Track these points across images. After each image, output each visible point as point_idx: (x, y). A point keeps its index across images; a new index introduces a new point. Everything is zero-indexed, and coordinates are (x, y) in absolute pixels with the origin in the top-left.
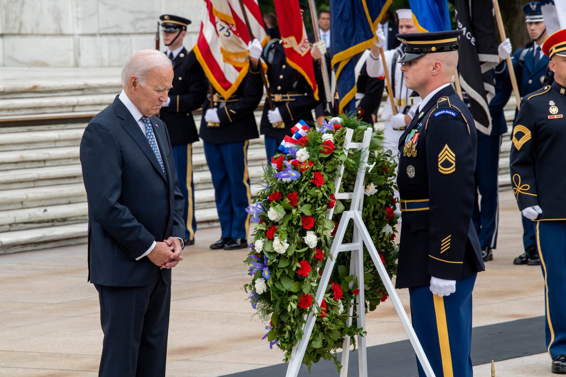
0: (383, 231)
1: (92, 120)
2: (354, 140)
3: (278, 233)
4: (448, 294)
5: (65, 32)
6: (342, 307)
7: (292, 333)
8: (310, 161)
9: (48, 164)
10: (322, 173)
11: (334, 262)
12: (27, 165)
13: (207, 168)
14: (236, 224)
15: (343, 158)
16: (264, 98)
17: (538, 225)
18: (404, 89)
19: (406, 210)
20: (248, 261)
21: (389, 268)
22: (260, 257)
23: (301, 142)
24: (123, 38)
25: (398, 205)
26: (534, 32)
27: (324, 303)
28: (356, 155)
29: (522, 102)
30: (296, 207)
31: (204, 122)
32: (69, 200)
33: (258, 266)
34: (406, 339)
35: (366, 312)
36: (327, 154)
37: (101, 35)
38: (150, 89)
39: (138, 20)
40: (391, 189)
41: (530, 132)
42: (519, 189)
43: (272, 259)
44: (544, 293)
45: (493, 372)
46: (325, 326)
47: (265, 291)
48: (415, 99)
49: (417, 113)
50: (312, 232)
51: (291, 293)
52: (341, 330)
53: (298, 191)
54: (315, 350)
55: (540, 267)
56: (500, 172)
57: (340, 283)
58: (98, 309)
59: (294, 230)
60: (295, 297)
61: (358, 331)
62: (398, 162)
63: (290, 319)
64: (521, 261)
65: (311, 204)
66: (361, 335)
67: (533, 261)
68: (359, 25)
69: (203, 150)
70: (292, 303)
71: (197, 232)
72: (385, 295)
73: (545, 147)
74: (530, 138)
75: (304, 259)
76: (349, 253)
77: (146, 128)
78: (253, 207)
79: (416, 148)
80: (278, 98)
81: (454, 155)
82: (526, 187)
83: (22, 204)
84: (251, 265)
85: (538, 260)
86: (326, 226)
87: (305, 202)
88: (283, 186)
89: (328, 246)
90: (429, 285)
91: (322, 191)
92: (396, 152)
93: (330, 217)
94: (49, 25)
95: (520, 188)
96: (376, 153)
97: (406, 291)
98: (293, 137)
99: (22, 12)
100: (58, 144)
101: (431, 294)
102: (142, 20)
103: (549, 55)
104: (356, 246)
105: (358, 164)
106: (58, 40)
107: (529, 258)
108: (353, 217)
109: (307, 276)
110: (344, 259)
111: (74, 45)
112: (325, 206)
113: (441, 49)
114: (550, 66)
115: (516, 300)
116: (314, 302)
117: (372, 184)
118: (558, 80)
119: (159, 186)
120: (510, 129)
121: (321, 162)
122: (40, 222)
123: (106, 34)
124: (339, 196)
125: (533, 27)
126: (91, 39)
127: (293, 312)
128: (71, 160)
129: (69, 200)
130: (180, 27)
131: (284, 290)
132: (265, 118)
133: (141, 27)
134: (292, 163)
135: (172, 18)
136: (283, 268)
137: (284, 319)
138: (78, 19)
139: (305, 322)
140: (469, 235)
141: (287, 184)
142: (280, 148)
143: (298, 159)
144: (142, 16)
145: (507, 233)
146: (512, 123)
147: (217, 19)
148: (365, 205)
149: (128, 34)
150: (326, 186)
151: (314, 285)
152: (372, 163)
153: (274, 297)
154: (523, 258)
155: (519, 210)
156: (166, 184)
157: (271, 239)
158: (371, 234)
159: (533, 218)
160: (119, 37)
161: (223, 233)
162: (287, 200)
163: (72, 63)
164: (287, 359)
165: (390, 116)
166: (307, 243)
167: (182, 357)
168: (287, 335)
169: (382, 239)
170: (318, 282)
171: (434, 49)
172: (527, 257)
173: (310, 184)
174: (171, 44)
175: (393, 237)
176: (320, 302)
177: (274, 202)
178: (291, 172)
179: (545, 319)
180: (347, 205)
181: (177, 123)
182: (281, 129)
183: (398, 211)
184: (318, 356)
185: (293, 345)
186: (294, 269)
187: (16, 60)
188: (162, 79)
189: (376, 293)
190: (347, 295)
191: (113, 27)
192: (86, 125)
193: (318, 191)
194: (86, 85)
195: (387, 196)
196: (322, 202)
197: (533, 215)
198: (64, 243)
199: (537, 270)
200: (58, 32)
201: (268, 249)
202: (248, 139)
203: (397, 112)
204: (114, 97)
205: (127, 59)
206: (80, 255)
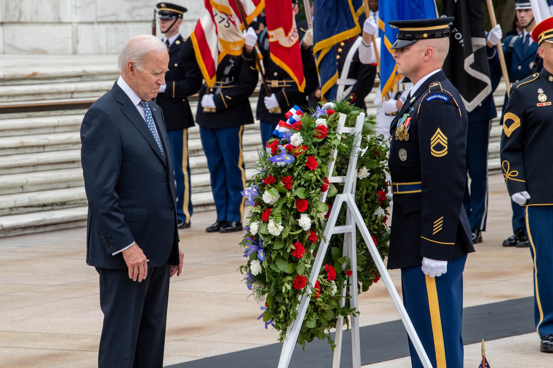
0: (376, 213)
2: (347, 124)
3: (273, 216)
4: (440, 275)
5: (63, 20)
6: (335, 287)
7: (286, 313)
8: (304, 146)
9: (47, 149)
10: (316, 157)
11: (328, 243)
12: (27, 150)
13: (203, 153)
14: (231, 207)
15: (336, 142)
16: (259, 84)
17: (527, 208)
19: (398, 193)
20: (243, 243)
21: (381, 250)
22: (255, 239)
23: (295, 126)
24: (120, 26)
25: (389, 188)
26: (524, 19)
27: (318, 284)
28: (349, 139)
29: (512, 89)
30: (290, 190)
31: (200, 108)
33: (254, 248)
35: (359, 293)
36: (321, 139)
37: (99, 23)
39: (134, 8)
40: (383, 172)
41: (519, 120)
42: (508, 175)
43: (267, 241)
46: (319, 306)
47: (261, 272)
48: (406, 84)
49: (409, 97)
50: (306, 215)
51: (285, 275)
52: (335, 310)
53: (292, 174)
54: (309, 330)
55: (529, 249)
56: (490, 156)
57: (333, 264)
58: (98, 290)
59: (288, 213)
60: (289, 278)
61: (351, 311)
62: (389, 146)
63: (284, 299)
64: (509, 243)
65: (305, 187)
66: (354, 315)
67: (522, 243)
68: (342, 15)
69: (199, 136)
70: (286, 284)
71: (193, 215)
72: (377, 276)
73: (534, 134)
74: (519, 125)
75: (298, 241)
76: (342, 235)
77: (145, 112)
78: (249, 191)
79: (409, 132)
80: (275, 84)
81: (446, 139)
82: (515, 173)
83: (22, 189)
84: (247, 247)
85: (528, 242)
86: (320, 209)
88: (277, 170)
89: (322, 228)
90: (421, 265)
91: (315, 175)
92: (387, 136)
93: (324, 200)
94: (48, 13)
95: (509, 175)
96: (369, 137)
98: (288, 122)
100: (57, 130)
102: (139, 8)
103: (538, 42)
104: (349, 229)
105: (350, 149)
107: (518, 239)
108: (346, 200)
109: (301, 257)
110: (337, 241)
111: (73, 33)
113: (432, 35)
114: (539, 52)
116: (308, 283)
117: (365, 168)
118: (546, 67)
119: (160, 169)
120: (499, 114)
121: (315, 146)
122: (39, 206)
123: (104, 22)
124: (332, 179)
125: (523, 14)
126: (89, 27)
127: (288, 293)
129: (68, 185)
130: (176, 15)
131: (279, 271)
132: (261, 104)
133: (137, 15)
134: (287, 148)
135: (168, 5)
136: (278, 250)
137: (279, 300)
138: (76, 7)
139: (299, 303)
140: (461, 218)
141: (281, 168)
142: (274, 133)
143: (292, 143)
145: (496, 216)
146: (501, 108)
148: (357, 189)
149: (125, 22)
150: (319, 170)
151: (308, 266)
152: (365, 147)
153: (268, 278)
154: (512, 240)
155: (508, 194)
156: (166, 168)
157: (266, 222)
158: (364, 217)
159: (522, 203)
160: (116, 26)
161: (218, 217)
162: (281, 184)
163: (70, 50)
164: (282, 339)
166: (301, 226)
168: (282, 315)
169: (374, 222)
170: (312, 263)
172: (516, 239)
173: (304, 168)
174: (168, 32)
175: (385, 219)
176: (314, 283)
177: (269, 185)
178: (285, 156)
179: (534, 299)
180: (340, 188)
181: (173, 109)
183: (390, 194)
184: (312, 336)
186: (289, 251)
187: (16, 48)
188: (158, 62)
189: (369, 274)
190: (340, 276)
191: (110, 16)
192: (85, 111)
193: (312, 175)
194: (84, 72)
197: (521, 200)
198: (63, 226)
200: (57, 21)
201: (263, 231)
202: (244, 124)
203: (389, 98)
204: (112, 83)
205: (122, 47)
206: (79, 239)
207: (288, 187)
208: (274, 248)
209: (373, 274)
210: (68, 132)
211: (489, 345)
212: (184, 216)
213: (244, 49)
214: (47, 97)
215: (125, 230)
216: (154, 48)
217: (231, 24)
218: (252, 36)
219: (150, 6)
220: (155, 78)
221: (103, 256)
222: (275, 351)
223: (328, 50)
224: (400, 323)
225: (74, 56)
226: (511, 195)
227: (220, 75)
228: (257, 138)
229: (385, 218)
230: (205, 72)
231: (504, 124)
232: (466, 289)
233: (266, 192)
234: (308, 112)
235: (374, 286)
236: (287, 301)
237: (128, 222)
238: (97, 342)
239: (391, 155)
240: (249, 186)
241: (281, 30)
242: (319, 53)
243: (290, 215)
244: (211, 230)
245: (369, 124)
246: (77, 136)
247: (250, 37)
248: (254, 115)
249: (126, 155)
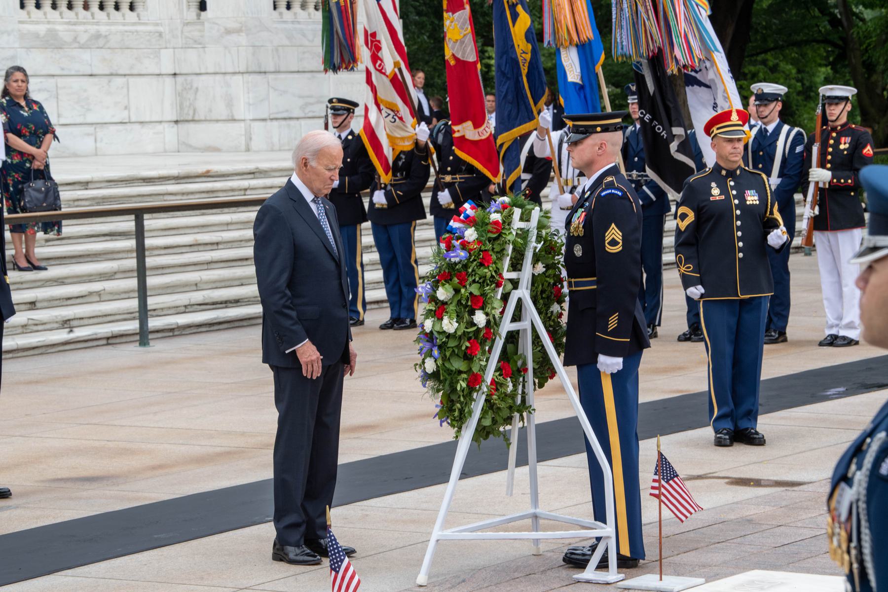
0: (551, 309)
1: (265, 203)
2: (521, 219)
3: (447, 312)
4: (615, 371)
5: (236, 117)
6: (511, 385)
7: (461, 411)
8: (479, 241)
9: (220, 246)
10: (491, 253)
11: (503, 340)
12: (201, 248)
13: (375, 249)
14: (404, 304)
15: (511, 238)
18: (571, 169)
19: (574, 289)
20: (418, 340)
21: (557, 346)
22: (430, 337)
23: (470, 221)
24: (292, 123)
25: (565, 284)
28: (524, 234)
30: (465, 286)
31: (372, 204)
32: (241, 282)
33: (428, 346)
34: (574, 415)
35: (535, 390)
38: (321, 168)
39: (307, 104)
40: (559, 268)
42: (683, 269)
45: (658, 446)
46: (494, 404)
48: (581, 178)
49: (584, 192)
50: (481, 312)
51: (460, 372)
52: (510, 408)
55: (703, 343)
56: (664, 251)
57: (508, 361)
58: (272, 388)
60: (465, 376)
61: (527, 408)
62: (564, 241)
63: (459, 397)
64: (684, 338)
66: (530, 412)
68: (523, 107)
69: (371, 232)
70: (461, 382)
71: (367, 312)
72: (553, 373)
76: (518, 332)
78: (422, 288)
79: (583, 227)
80: (448, 178)
83: (197, 286)
84: (421, 345)
86: (495, 305)
87: (474, 281)
88: (451, 266)
89: (497, 324)
90: (597, 362)
92: (563, 231)
93: (499, 297)
94: (221, 110)
96: (544, 232)
97: (574, 369)
98: (462, 217)
99: (195, 99)
100: (230, 227)
101: (599, 372)
102: (311, 104)
104: (524, 325)
106: (230, 125)
107: (693, 334)
108: (521, 296)
110: (513, 337)
112: (493, 285)
113: (606, 129)
116: (484, 381)
117: (540, 263)
119: (331, 266)
120: (673, 208)
121: (489, 241)
122: (213, 304)
123: (276, 119)
124: (508, 275)
127: (463, 391)
129: (241, 282)
130: (348, 110)
132: (435, 199)
134: (462, 244)
135: (340, 101)
137: (454, 397)
138: (249, 104)
139: (475, 401)
140: (636, 313)
141: (456, 264)
142: (448, 228)
143: (466, 239)
144: (311, 100)
147: (382, 107)
148: (533, 284)
149: (298, 119)
151: (483, 363)
152: (540, 242)
155: (682, 289)
156: (338, 265)
157: (441, 319)
158: (540, 313)
159: (696, 298)
160: (288, 122)
161: (392, 314)
163: (243, 147)
164: (457, 437)
165: (557, 196)
167: (353, 435)
168: (456, 414)
169: (550, 318)
170: (487, 360)
171: (599, 129)
172: (691, 334)
174: (340, 127)
175: (560, 315)
176: (489, 381)
180: (515, 284)
181: (346, 204)
182: (451, 210)
183: (566, 290)
184: (488, 434)
185: (463, 423)
186: (463, 348)
187: (190, 146)
188: (332, 157)
189: (545, 371)
190: (516, 373)
191: (282, 112)
192: (258, 208)
193: (486, 270)
195: (555, 275)
197: (696, 294)
198: (237, 324)
199: (702, 345)
201: (437, 328)
202: (415, 220)
204: (285, 180)
205: (297, 142)
206: (254, 336)
207: (462, 283)
209: (549, 372)
211: (664, 439)
212: (358, 313)
213: (417, 143)
214: (220, 194)
215: (298, 328)
217: (397, 120)
218: (425, 131)
219: (322, 102)
220: (328, 174)
221: (280, 358)
222: (450, 449)
223: (510, 143)
224: (575, 420)
227: (396, 169)
228: (431, 233)
229: (561, 314)
230: (380, 170)
232: (641, 385)
233: (440, 289)
234: (483, 208)
236: (462, 399)
237: (300, 320)
238: (273, 440)
239: (567, 251)
240: (423, 282)
241: (469, 124)
242: (502, 145)
244: (384, 327)
245: (544, 219)
246: (250, 233)
247: (423, 132)
248: (427, 210)
249: (297, 252)
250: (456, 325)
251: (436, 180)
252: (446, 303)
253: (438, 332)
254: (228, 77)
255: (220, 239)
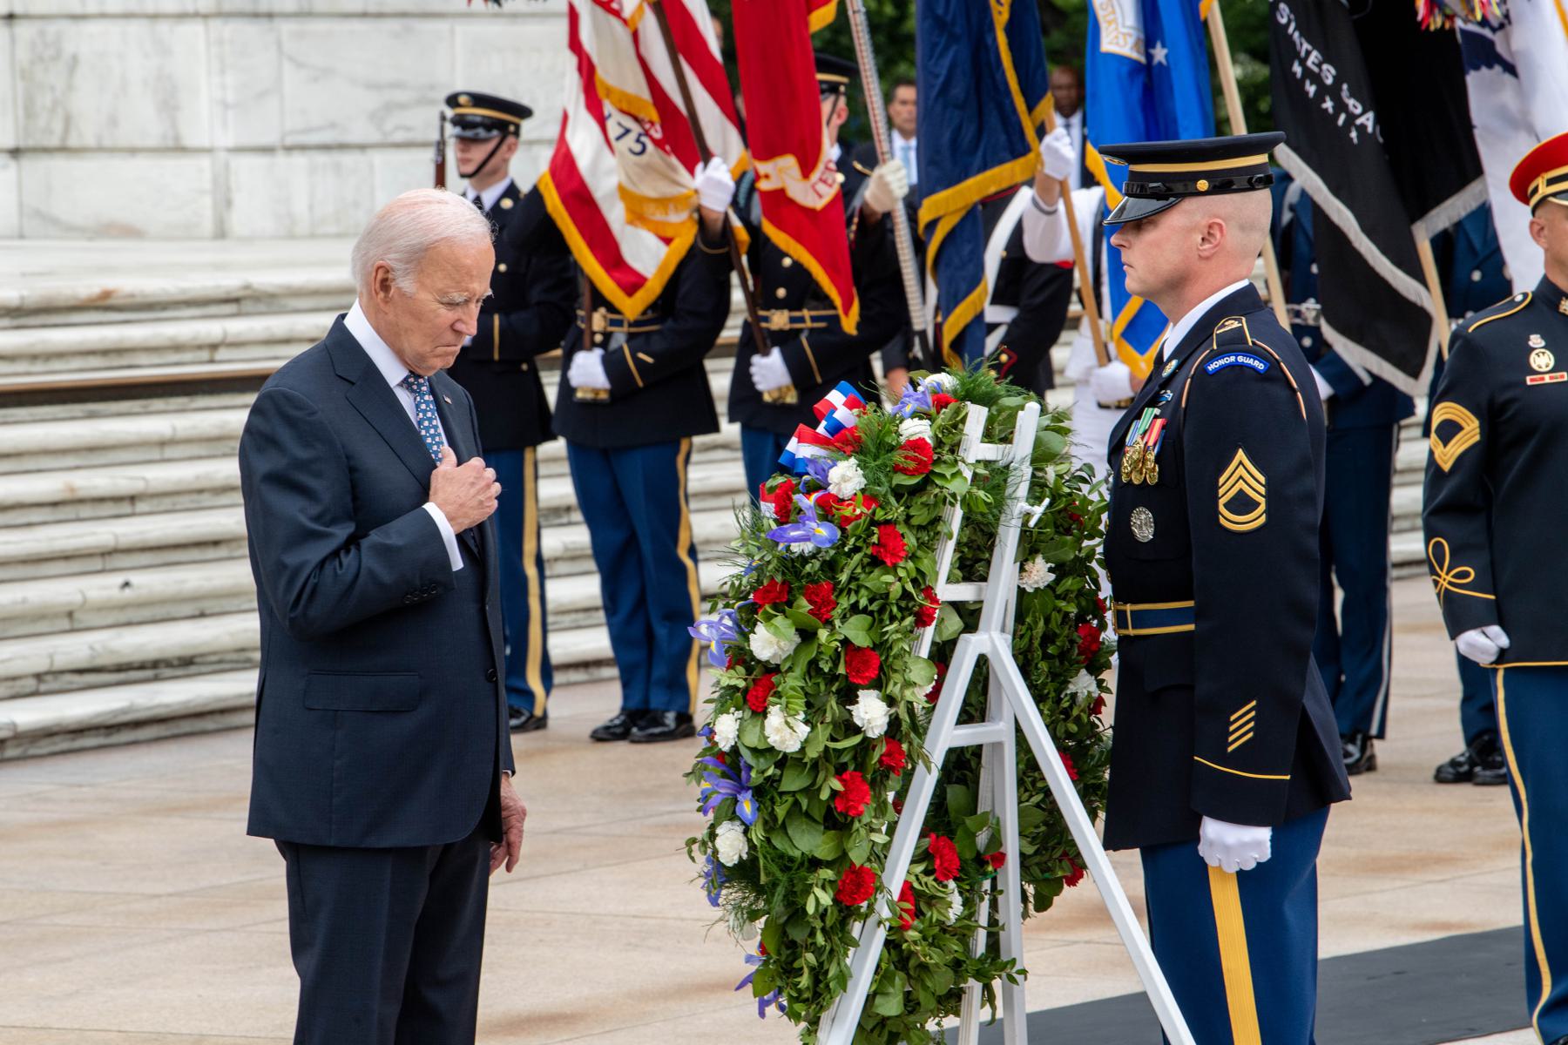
2: (988, 436)
5: (189, 141)
6: (957, 901)
7: (818, 974)
8: (869, 497)
9: (141, 506)
12: (86, 511)
14: (659, 671)
17: (1500, 675)
20: (696, 773)
22: (730, 764)
23: (842, 441)
24: (348, 159)
27: (908, 891)
28: (994, 478)
30: (828, 623)
33: (725, 788)
36: (915, 475)
37: (289, 149)
38: (427, 299)
39: (390, 107)
41: (1477, 423)
44: (1519, 863)
47: (745, 857)
51: (815, 863)
53: (834, 578)
54: (884, 1021)
55: (1505, 791)
56: (1395, 526)
57: (951, 834)
59: (823, 687)
60: (827, 874)
64: (1454, 774)
65: (871, 613)
67: (1488, 773)
69: (565, 468)
70: (818, 891)
72: (1077, 869)
74: (1477, 438)
75: (851, 768)
76: (977, 751)
77: (417, 406)
80: (779, 320)
81: (1262, 479)
83: (71, 620)
85: (1504, 770)
87: (854, 609)
91: (900, 579)
93: (924, 652)
94: (145, 124)
96: (1051, 472)
98: (821, 429)
102: (402, 106)
104: (994, 732)
105: (999, 506)
107: (1477, 763)
108: (986, 650)
109: (860, 814)
110: (963, 767)
111: (215, 180)
115: (1442, 881)
122: (119, 668)
123: (303, 148)
124: (948, 591)
128: (205, 496)
130: (502, 126)
132: (742, 378)
133: (398, 128)
135: (479, 100)
136: (793, 793)
137: (798, 935)
138: (226, 106)
141: (804, 559)
143: (832, 489)
144: (401, 96)
145: (1416, 697)
148: (1020, 618)
149: (362, 147)
150: (910, 565)
151: (880, 838)
153: (767, 874)
157: (761, 713)
158: (1039, 699)
159: (1485, 660)
162: (804, 605)
163: (208, 226)
166: (859, 723)
168: (805, 981)
169: (1067, 713)
170: (891, 831)
173: (866, 560)
176: (896, 888)
177: (768, 608)
178: (813, 525)
179: (1522, 935)
180: (970, 616)
187: (54, 221)
188: (459, 272)
189: (1054, 862)
191: (319, 129)
193: (889, 578)
194: (247, 287)
196: (900, 608)
197: (1484, 651)
198: (186, 726)
200: (170, 143)
201: (752, 739)
208: (783, 788)
210: (200, 458)
212: (529, 695)
216: (432, 237)
225: (218, 244)
226: (1453, 637)
228: (734, 473)
231: (1433, 435)
235: (1068, 895)
243: (829, 692)
244: (605, 735)
250: (803, 730)
251: (746, 326)
252: (776, 670)
253: (755, 751)
254: (163, 27)
255: (136, 486)
